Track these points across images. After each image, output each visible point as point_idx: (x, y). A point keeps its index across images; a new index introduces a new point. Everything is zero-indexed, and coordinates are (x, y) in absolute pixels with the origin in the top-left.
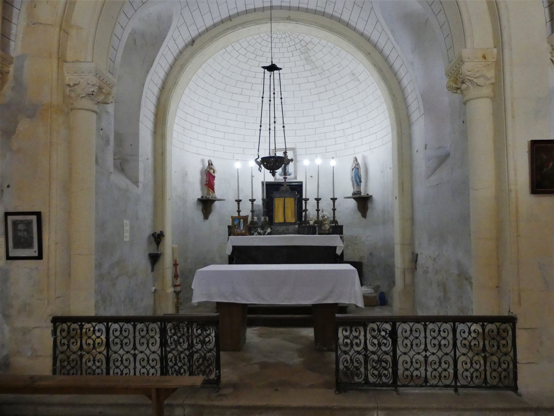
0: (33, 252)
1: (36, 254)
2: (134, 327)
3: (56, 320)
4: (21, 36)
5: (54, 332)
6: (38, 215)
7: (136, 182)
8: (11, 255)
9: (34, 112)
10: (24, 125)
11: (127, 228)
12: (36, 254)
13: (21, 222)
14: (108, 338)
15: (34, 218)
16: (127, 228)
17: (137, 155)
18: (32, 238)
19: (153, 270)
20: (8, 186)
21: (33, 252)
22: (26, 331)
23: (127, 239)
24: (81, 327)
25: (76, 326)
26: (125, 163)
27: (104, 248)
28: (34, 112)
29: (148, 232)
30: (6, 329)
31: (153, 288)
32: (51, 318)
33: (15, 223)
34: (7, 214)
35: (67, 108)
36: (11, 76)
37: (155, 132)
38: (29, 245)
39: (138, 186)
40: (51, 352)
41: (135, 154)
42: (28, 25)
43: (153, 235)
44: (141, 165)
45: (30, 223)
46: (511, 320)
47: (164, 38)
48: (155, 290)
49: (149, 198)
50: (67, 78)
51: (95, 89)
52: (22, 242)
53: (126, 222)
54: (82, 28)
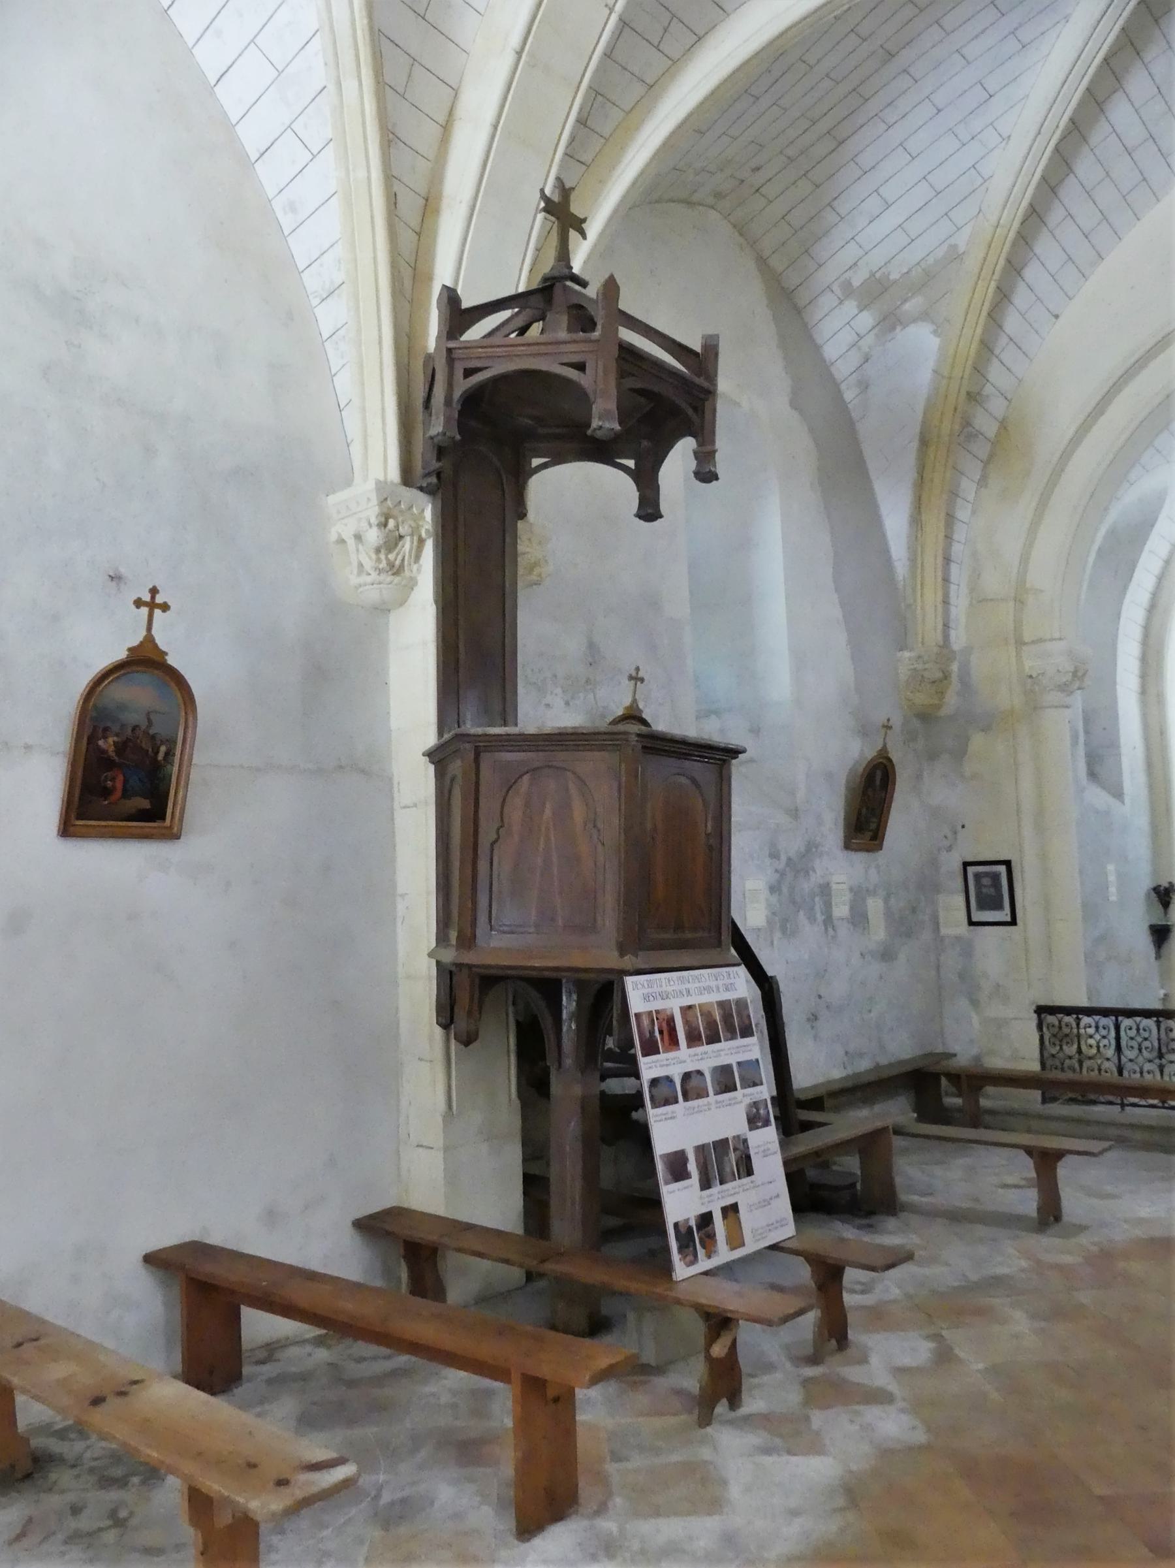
0: (1004, 915)
1: (1009, 919)
2: (1158, 1023)
3: (1042, 1011)
4: (963, 620)
5: (1040, 1027)
6: (1008, 864)
7: (1118, 795)
8: (974, 919)
9: (988, 723)
10: (978, 741)
11: (1112, 878)
12: (1009, 919)
13: (986, 874)
14: (1118, 1038)
15: (1002, 869)
16: (1112, 878)
17: (1118, 747)
18: (1002, 896)
19: (1158, 956)
20: (963, 827)
21: (1004, 915)
22: (1001, 1023)
23: (1113, 898)
24: (1078, 1020)
25: (1067, 1019)
26: (1099, 763)
27: (1091, 911)
28: (988, 723)
29: (1144, 883)
30: (975, 1020)
31: (1162, 992)
32: (1034, 1007)
33: (977, 876)
34: (966, 865)
35: (1034, 707)
36: (954, 678)
37: (1143, 692)
38: (999, 906)
39: (1123, 803)
40: (1037, 1054)
41: (1113, 745)
42: (971, 604)
43: (1156, 890)
44: (1126, 762)
45: (977, 876)
46: (721, 757)
47: (1153, 526)
48: (1165, 995)
49: (1141, 821)
50: (1027, 668)
51: (1069, 677)
52: (990, 902)
53: (1111, 868)
54: (1042, 591)
